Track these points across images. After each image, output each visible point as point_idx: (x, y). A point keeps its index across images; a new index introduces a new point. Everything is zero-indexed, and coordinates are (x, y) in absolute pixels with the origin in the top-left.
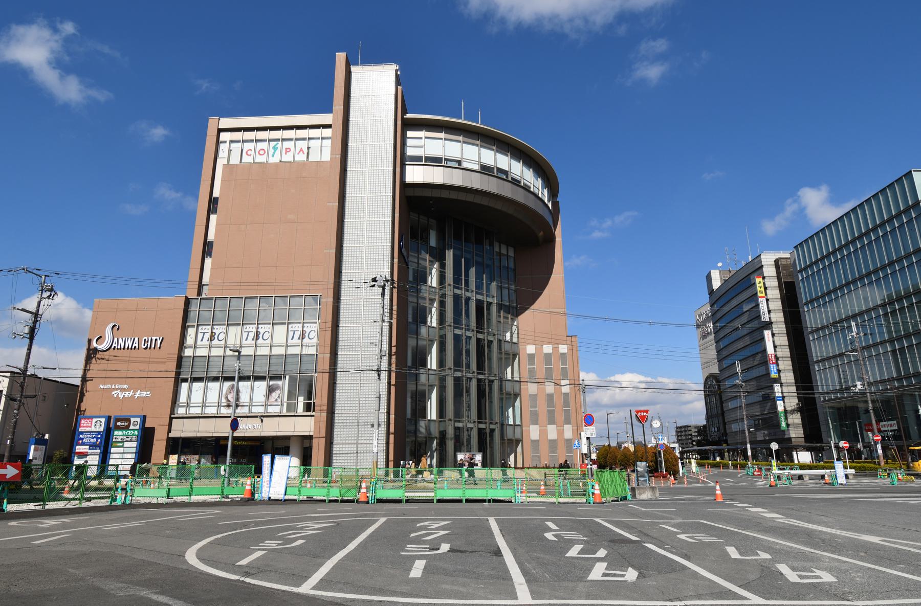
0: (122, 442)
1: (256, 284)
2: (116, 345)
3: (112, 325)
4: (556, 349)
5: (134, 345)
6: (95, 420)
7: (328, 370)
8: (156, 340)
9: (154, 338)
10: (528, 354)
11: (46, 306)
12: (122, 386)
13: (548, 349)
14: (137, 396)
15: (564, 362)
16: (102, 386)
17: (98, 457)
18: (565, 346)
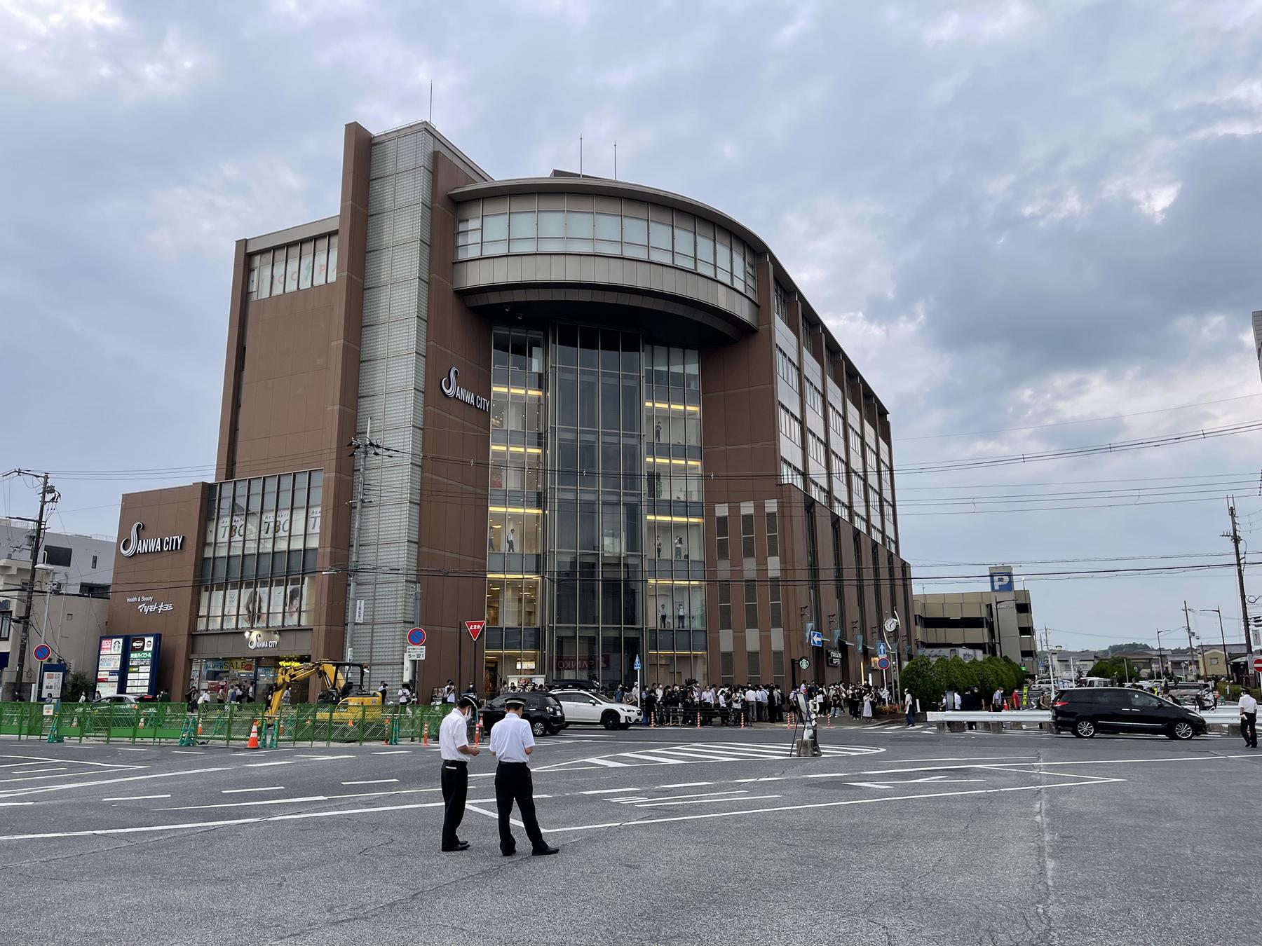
0: (138, 666)
1: (283, 459)
2: (140, 549)
3: (136, 525)
4: (759, 507)
5: (157, 547)
6: (114, 640)
7: (192, 582)
8: (177, 539)
10: (743, 516)
11: (50, 510)
12: (147, 599)
13: (747, 508)
14: (160, 610)
15: (772, 528)
16: (129, 600)
17: (117, 683)
18: (751, 504)
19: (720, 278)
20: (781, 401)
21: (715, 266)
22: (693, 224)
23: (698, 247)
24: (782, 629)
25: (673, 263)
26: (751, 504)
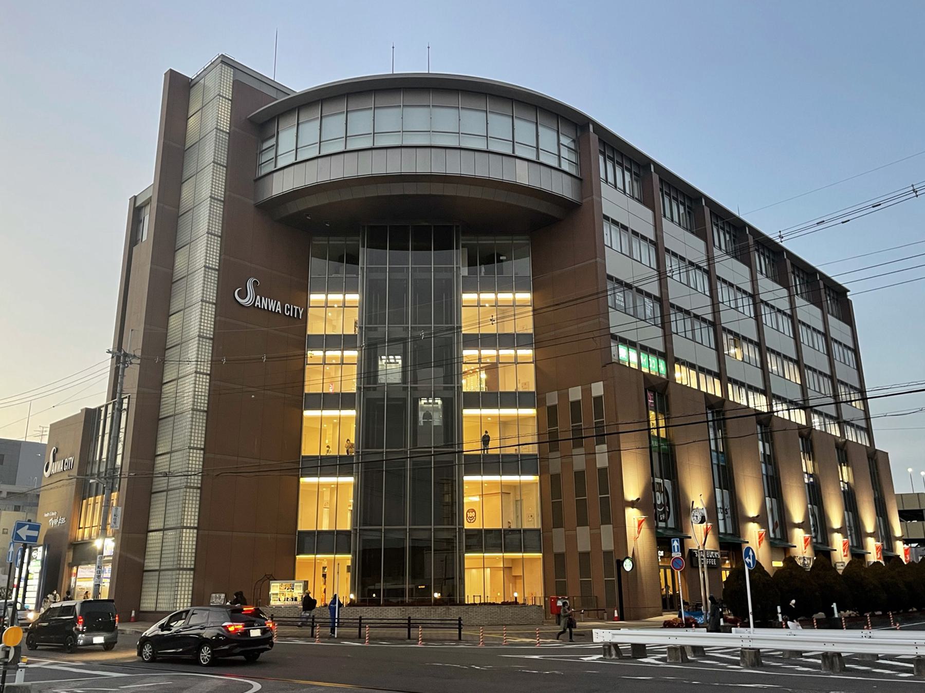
2: (259, 304)
5: (277, 309)
8: (298, 310)
9: (296, 308)
13: (575, 394)
18: (601, 384)
19: (543, 159)
20: (800, 319)
21: (537, 148)
22: (556, 122)
23: (540, 137)
24: (611, 526)
25: (513, 152)
26: (601, 384)
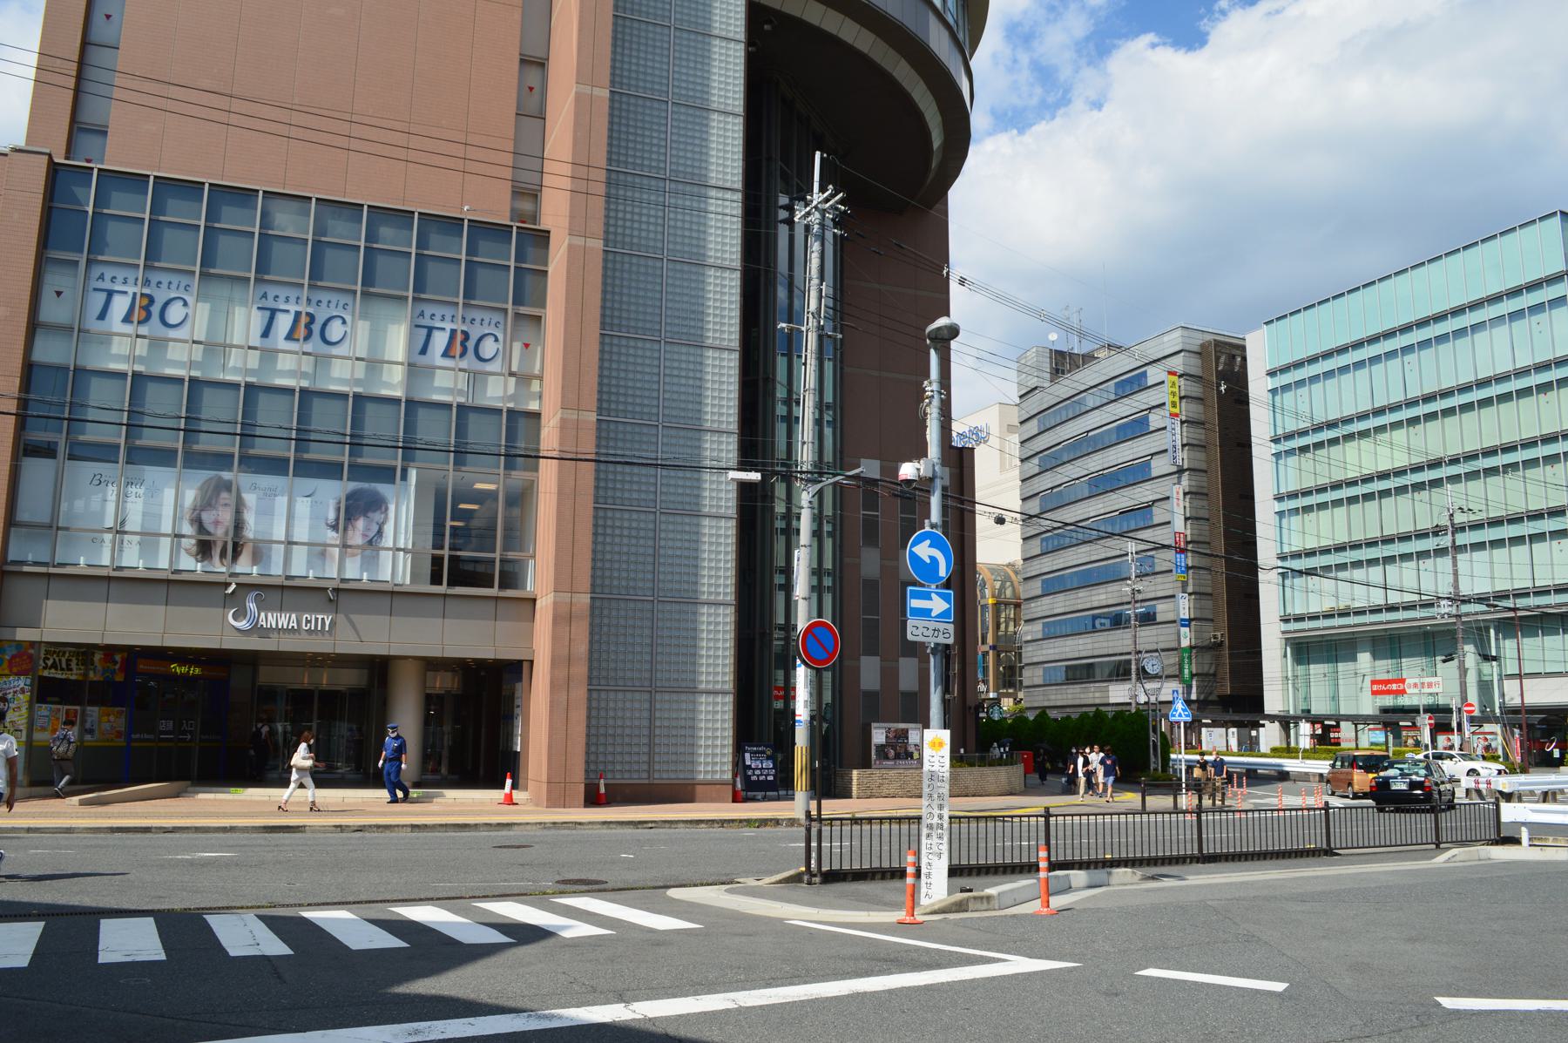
5: (291, 625)
8: (323, 619)
24: (878, 658)
